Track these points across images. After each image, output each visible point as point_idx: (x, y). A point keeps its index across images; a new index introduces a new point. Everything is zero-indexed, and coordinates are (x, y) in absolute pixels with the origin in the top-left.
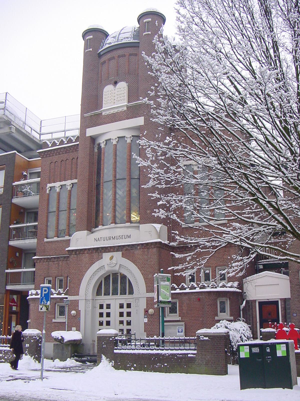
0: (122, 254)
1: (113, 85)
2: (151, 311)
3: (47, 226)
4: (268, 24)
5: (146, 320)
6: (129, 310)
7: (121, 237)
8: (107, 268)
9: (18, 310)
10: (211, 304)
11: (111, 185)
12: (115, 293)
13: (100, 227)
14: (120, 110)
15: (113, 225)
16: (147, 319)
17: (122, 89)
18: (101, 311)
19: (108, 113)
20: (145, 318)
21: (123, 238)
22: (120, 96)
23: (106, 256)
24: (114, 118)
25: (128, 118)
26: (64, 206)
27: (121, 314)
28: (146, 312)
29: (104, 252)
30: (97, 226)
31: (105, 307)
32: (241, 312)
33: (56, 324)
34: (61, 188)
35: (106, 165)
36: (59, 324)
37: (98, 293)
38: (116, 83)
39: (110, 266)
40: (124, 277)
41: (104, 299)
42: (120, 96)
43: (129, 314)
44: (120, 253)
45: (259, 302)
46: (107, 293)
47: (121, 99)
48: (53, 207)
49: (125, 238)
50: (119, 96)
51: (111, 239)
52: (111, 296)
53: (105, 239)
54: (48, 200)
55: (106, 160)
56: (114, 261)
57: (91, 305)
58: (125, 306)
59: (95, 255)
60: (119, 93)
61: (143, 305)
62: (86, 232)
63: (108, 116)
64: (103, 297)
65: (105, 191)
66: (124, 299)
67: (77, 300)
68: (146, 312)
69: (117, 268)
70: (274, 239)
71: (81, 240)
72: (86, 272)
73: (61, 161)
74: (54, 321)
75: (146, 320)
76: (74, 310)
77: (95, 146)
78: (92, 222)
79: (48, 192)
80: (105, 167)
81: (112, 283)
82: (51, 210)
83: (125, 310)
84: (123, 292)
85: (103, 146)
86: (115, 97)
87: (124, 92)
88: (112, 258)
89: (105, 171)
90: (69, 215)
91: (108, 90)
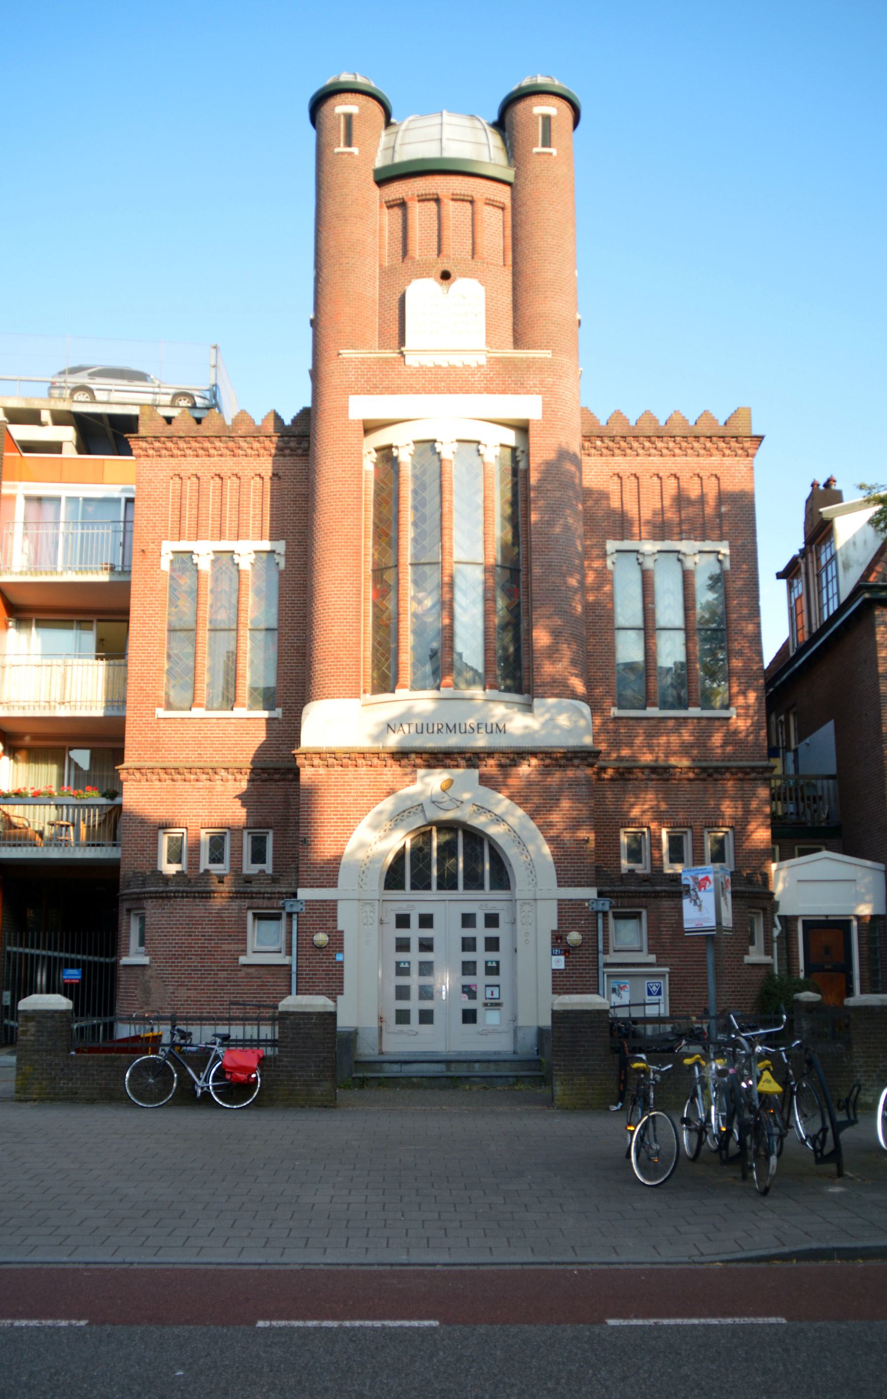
2: (574, 937)
4: (825, 601)
5: (559, 962)
6: (469, 933)
16: (562, 958)
19: (428, 361)
20: (553, 954)
24: (445, 381)
28: (557, 938)
31: (414, 921)
32: (775, 945)
33: (252, 970)
36: (263, 971)
40: (475, 838)
41: (414, 901)
43: (492, 944)
45: (804, 922)
51: (444, 730)
52: (434, 893)
58: (480, 920)
63: (422, 370)
64: (408, 893)
67: (330, 901)
68: (557, 938)
70: (701, 1029)
74: (243, 960)
75: (559, 962)
84: (474, 881)
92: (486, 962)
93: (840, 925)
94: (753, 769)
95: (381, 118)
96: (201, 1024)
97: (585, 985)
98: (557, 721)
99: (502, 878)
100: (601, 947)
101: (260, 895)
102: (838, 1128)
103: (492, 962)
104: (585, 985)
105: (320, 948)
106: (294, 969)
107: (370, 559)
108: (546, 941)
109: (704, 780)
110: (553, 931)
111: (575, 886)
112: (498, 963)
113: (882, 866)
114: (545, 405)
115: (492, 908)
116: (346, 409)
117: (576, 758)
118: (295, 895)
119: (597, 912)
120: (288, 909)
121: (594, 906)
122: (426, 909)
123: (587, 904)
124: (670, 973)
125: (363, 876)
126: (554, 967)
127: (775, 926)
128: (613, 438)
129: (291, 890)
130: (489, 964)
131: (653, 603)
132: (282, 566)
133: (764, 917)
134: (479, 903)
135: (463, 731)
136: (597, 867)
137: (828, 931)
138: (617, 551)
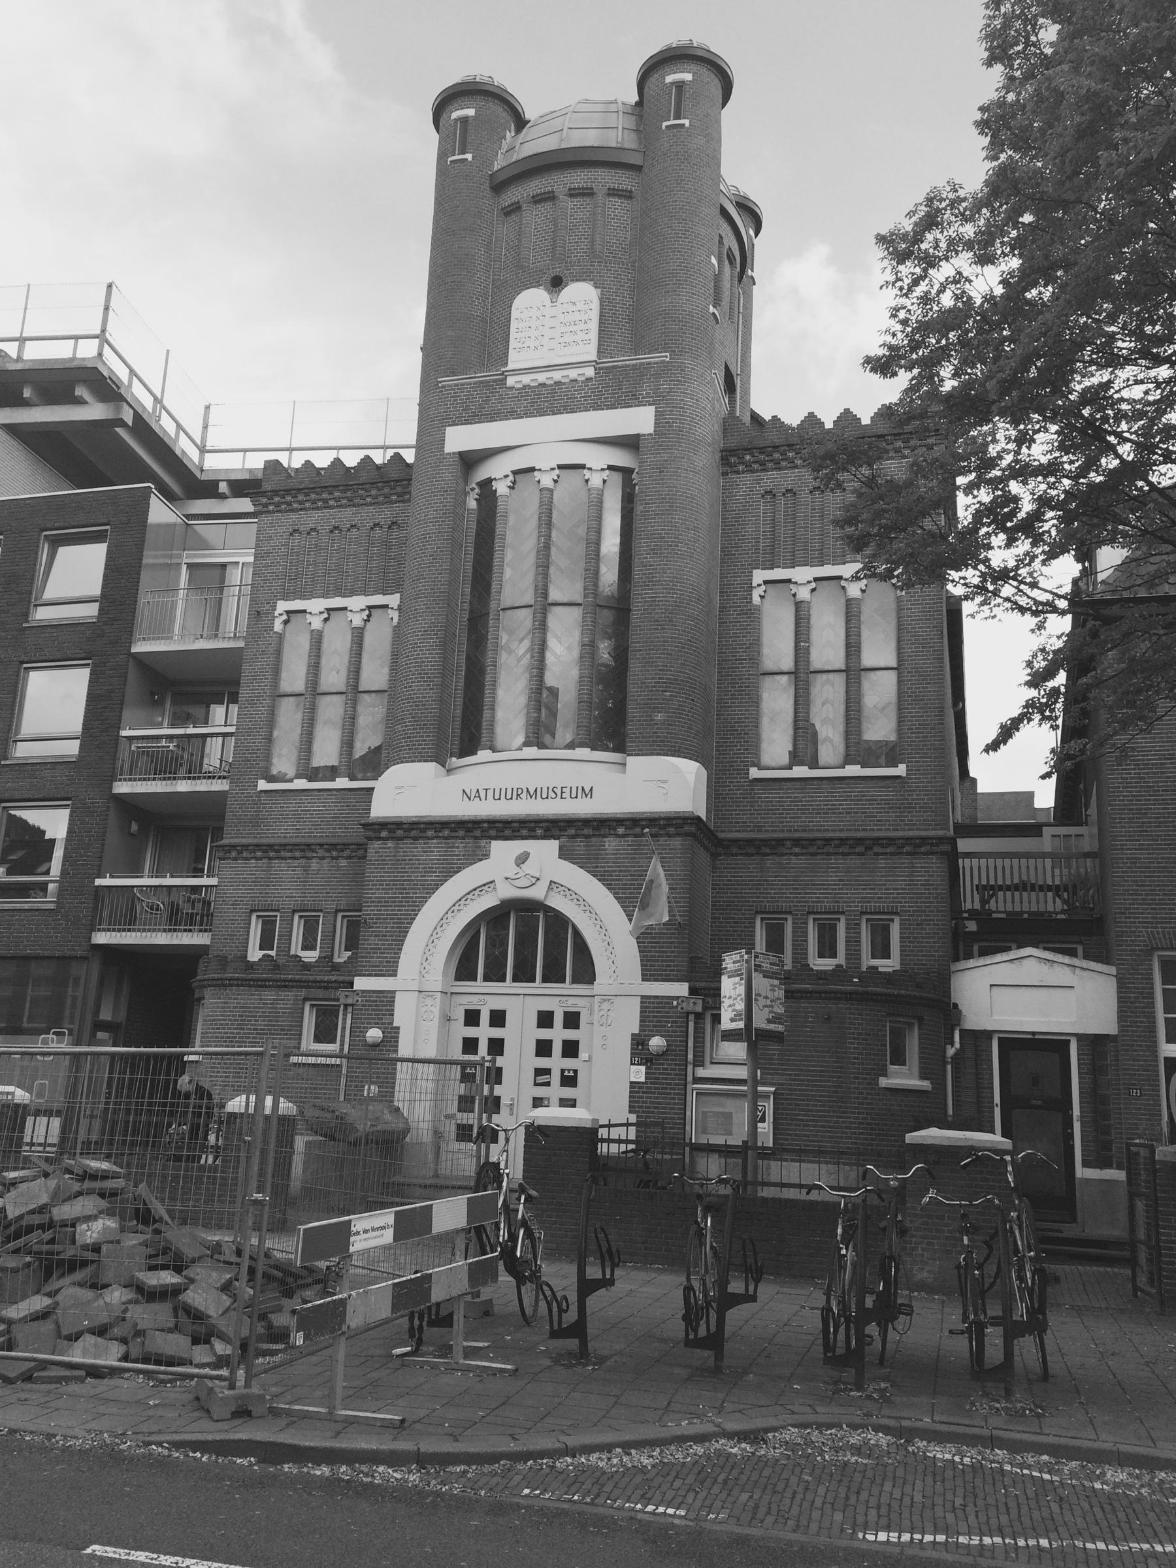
0: (561, 848)
1: (546, 289)
2: (657, 1042)
3: (269, 740)
5: (639, 1074)
6: (571, 1035)
7: (559, 793)
8: (507, 892)
9: (122, 1017)
10: (867, 1034)
11: (525, 618)
12: (524, 974)
13: (483, 755)
14: (573, 374)
15: (532, 751)
16: (643, 1068)
17: (580, 306)
18: (471, 1032)
19: (526, 379)
21: (566, 795)
22: (573, 328)
23: (503, 851)
24: (549, 400)
25: (596, 407)
26: (334, 676)
27: (543, 1048)
28: (638, 1044)
29: (497, 838)
30: (472, 752)
31: (485, 1018)
32: (949, 1067)
33: (301, 1070)
34: (326, 620)
35: (509, 555)
37: (464, 970)
38: (557, 284)
39: (516, 883)
40: (558, 923)
41: (485, 995)
42: (573, 328)
43: (571, 1049)
44: (551, 847)
45: (1001, 1041)
46: (495, 973)
47: (576, 338)
48: (294, 676)
49: (574, 795)
50: (568, 329)
51: (524, 796)
52: (509, 986)
53: (500, 795)
54: (279, 653)
55: (510, 537)
56: (529, 868)
57: (436, 1011)
58: (558, 1020)
59: (459, 847)
60: (570, 318)
61: (629, 1020)
62: (432, 766)
64: (480, 985)
65: (504, 638)
66: (558, 997)
68: (638, 1044)
69: (537, 893)
71: (410, 791)
72: (425, 899)
73: (331, 531)
75: (639, 1074)
76: (376, 1025)
77: (468, 489)
78: (462, 731)
79: (278, 626)
80: (507, 560)
81: (523, 942)
82: (285, 686)
83: (558, 1034)
84: (553, 974)
85: (501, 488)
86: (554, 329)
87: (586, 317)
88: (522, 859)
89: (508, 573)
90: (354, 709)
91: (530, 304)
92: (563, 1071)
93: (1055, 1046)
94: (924, 839)
95: (718, 93)
96: (800, 1161)
97: (669, 1104)
98: (668, 784)
99: (585, 972)
100: (690, 1057)
101: (318, 984)
102: (731, 1301)
103: (569, 1071)
104: (669, 1104)
105: (375, 1046)
106: (344, 1071)
107: (466, 606)
108: (625, 1048)
109: (862, 854)
110: (633, 1035)
111: (663, 980)
112: (576, 1071)
113: (1113, 970)
114: (658, 415)
115: (572, 1005)
116: (442, 441)
117: (672, 825)
118: (351, 984)
119: (688, 1013)
120: (342, 1001)
121: (684, 1005)
122: (498, 1004)
123: (675, 1003)
124: (774, 1093)
125: (425, 964)
126: (633, 1080)
127: (952, 1045)
128: (762, 450)
129: (348, 978)
130: (566, 1073)
131: (808, 640)
132: (396, 620)
133: (920, 1029)
134: (559, 998)
135: (544, 796)
136: (691, 958)
137: (1035, 1052)
138: (766, 582)
